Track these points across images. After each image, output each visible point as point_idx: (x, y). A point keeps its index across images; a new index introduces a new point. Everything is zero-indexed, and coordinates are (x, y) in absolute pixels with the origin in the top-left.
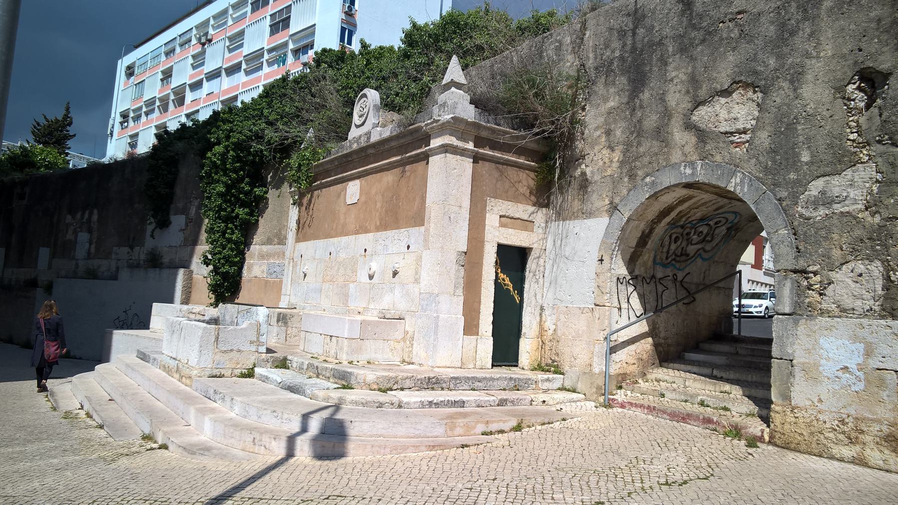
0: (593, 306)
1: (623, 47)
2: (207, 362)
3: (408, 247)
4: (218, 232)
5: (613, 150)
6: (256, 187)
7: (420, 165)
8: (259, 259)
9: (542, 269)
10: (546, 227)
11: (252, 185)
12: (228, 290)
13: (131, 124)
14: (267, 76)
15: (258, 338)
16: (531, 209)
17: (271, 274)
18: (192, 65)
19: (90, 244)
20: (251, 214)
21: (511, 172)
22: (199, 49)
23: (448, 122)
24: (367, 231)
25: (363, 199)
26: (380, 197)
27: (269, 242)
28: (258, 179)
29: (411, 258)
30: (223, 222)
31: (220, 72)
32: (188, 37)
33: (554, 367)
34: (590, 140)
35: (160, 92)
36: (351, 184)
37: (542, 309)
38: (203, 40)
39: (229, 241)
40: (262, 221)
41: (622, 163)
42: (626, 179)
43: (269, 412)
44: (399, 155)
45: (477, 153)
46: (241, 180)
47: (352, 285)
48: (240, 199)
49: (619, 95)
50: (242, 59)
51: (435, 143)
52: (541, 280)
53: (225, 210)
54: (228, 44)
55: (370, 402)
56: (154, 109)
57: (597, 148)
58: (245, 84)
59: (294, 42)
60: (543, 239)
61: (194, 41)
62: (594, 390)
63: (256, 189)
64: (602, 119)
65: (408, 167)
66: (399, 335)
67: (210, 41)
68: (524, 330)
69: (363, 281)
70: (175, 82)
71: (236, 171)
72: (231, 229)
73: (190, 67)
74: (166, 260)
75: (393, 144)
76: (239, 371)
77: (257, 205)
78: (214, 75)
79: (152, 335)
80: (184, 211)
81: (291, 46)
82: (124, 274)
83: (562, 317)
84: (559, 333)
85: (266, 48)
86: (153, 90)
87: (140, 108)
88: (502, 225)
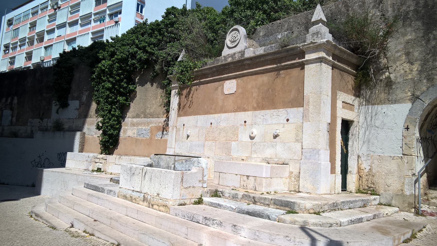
0: (402, 155)
1: (416, 4)
2: (177, 196)
3: (288, 120)
4: (106, 110)
5: (412, 64)
6: (130, 84)
7: (295, 72)
8: (131, 126)
9: (358, 133)
10: (359, 108)
11: (128, 83)
12: (111, 144)
13: (11, 51)
14: (94, 28)
15: (203, 178)
16: (353, 98)
17: (140, 135)
18: (48, 20)
19: (12, 117)
20: (126, 100)
21: (345, 75)
22: (53, 12)
23: (324, 43)
24: (245, 110)
25: (240, 91)
26: (256, 90)
27: (138, 116)
28: (131, 81)
29: (290, 127)
30: (109, 105)
31: (66, 24)
32: (46, 5)
33: (371, 191)
34: (392, 58)
35: (29, 34)
36: (227, 82)
37: (359, 157)
38: (55, 7)
39: (113, 115)
40: (132, 105)
41: (420, 72)
42: (425, 81)
43: (282, 237)
44: (273, 64)
45: (334, 63)
46: (122, 81)
47: (233, 143)
48: (120, 91)
49: (416, 32)
50: (79, 18)
51: (308, 57)
52: (357, 140)
53: (111, 98)
54: (70, 10)
55: (325, 224)
56: (25, 43)
57: (398, 63)
58: (80, 32)
59: (110, 10)
60: (358, 115)
61: (49, 8)
62: (407, 205)
63: (129, 86)
64: (402, 46)
65: (282, 72)
66: (287, 174)
67: (59, 8)
68: (349, 169)
69: (244, 140)
70: (38, 29)
71: (118, 75)
72: (114, 109)
73: (47, 22)
74: (66, 126)
75: (269, 57)
76: (194, 200)
77: (130, 95)
78: (62, 26)
79: (68, 171)
80: (78, 98)
81: (108, 12)
82: (38, 135)
83: (376, 161)
84: (374, 171)
85: (93, 12)
86: (24, 33)
87: (17, 43)
88: (343, 107)
